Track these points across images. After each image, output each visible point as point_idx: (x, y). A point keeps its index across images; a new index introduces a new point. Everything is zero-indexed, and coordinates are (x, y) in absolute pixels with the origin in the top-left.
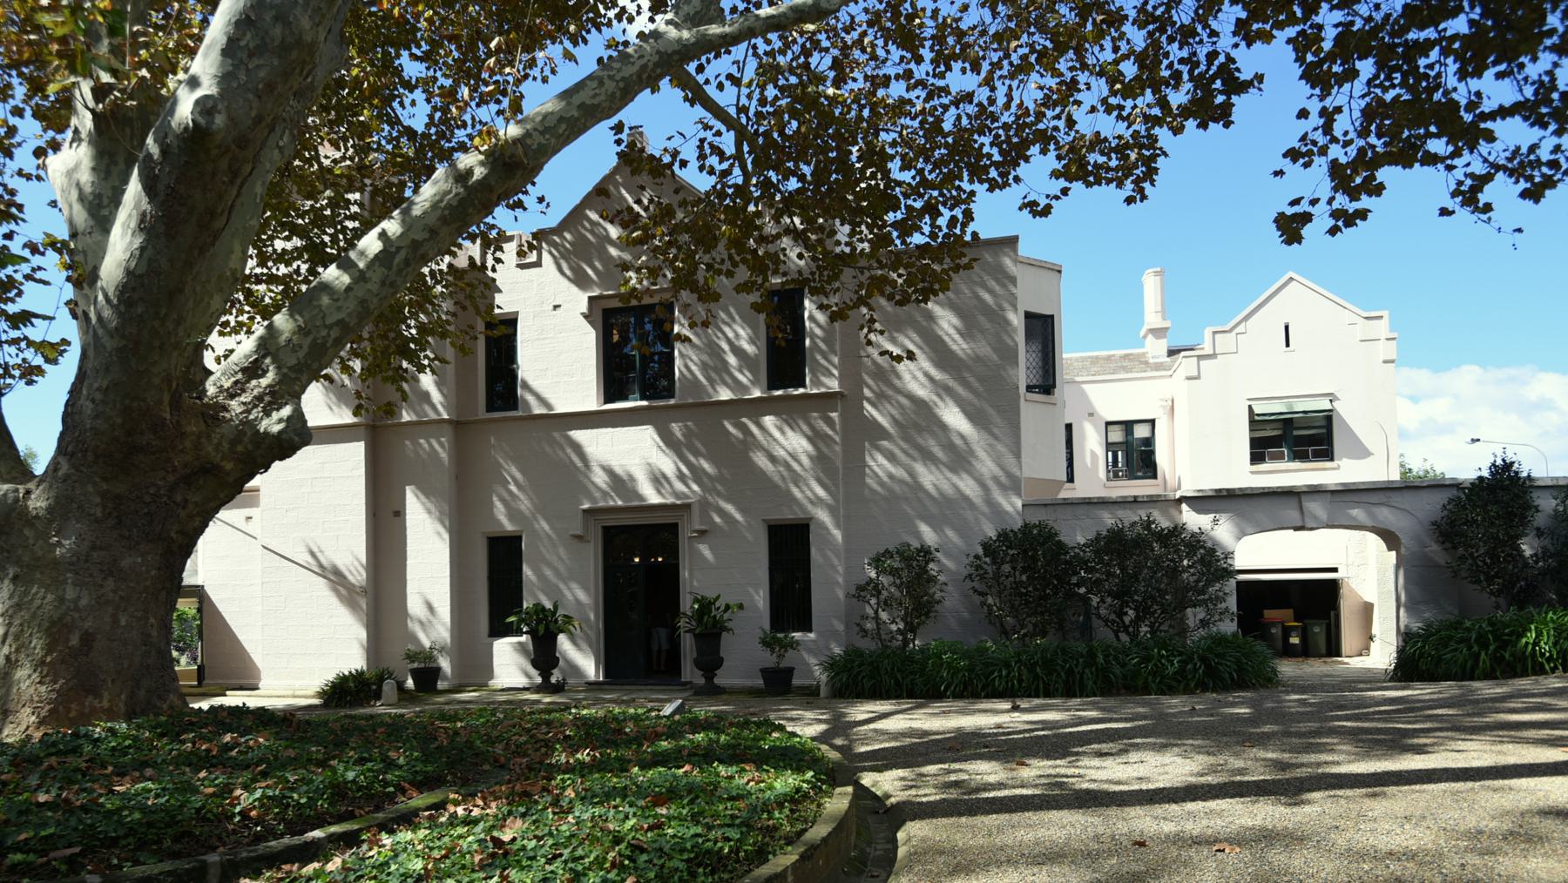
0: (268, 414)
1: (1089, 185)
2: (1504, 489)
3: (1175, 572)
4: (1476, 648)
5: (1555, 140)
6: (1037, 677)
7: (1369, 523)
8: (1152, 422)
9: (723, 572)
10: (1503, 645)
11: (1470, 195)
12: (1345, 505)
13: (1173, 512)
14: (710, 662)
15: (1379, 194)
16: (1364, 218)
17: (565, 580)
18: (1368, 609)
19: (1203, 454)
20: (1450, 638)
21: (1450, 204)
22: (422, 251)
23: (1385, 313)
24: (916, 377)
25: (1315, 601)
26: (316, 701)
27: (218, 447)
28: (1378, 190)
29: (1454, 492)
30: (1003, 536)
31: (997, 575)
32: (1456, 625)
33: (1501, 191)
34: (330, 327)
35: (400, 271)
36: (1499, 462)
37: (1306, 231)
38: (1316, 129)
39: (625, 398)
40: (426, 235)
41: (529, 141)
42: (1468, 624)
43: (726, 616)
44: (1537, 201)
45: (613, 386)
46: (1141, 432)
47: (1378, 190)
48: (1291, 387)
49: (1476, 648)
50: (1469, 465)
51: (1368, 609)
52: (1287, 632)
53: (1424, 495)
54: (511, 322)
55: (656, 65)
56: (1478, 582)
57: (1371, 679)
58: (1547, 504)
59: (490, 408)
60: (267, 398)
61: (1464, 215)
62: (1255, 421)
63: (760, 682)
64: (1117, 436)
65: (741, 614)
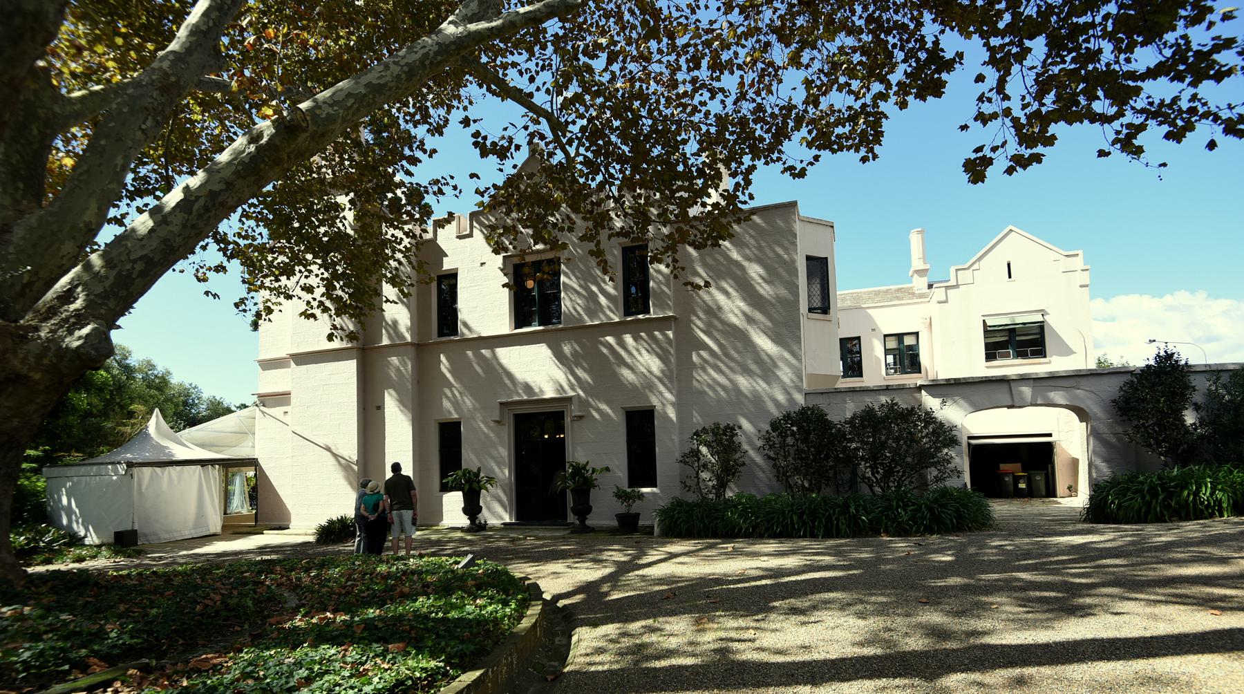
0: (71, 333)
1: (834, 151)
2: (1167, 376)
3: (912, 439)
4: (1148, 498)
5: (1191, 91)
6: (804, 523)
7: (1064, 402)
8: (917, 334)
9: (597, 448)
10: (1170, 495)
11: (1128, 144)
12: (1045, 388)
13: (917, 395)
14: (584, 510)
15: (1052, 144)
16: (1039, 161)
17: (491, 454)
18: (1075, 463)
19: (954, 352)
20: (1128, 489)
21: (1107, 148)
22: (220, 199)
23: (1080, 252)
24: (733, 307)
25: (1038, 456)
26: (312, 539)
27: (24, 361)
28: (1050, 141)
29: (1129, 377)
30: (787, 417)
31: (783, 445)
32: (1132, 479)
33: (1153, 136)
34: (135, 261)
35: (200, 216)
36: (1162, 353)
37: (990, 172)
38: (991, 90)
39: (530, 325)
40: (224, 187)
41: (318, 112)
42: (1141, 478)
43: (594, 476)
44: (1179, 142)
45: (521, 318)
46: (909, 341)
47: (1050, 141)
48: (1014, 305)
49: (1148, 498)
50: (1140, 357)
51: (1075, 463)
52: (1016, 480)
53: (1105, 379)
54: (453, 276)
55: (436, 53)
56: (1150, 445)
57: (1063, 523)
58: (1201, 385)
59: (441, 334)
60: (72, 320)
61: (1117, 154)
62: (988, 331)
63: (615, 523)
64: (892, 344)
65: (608, 474)
